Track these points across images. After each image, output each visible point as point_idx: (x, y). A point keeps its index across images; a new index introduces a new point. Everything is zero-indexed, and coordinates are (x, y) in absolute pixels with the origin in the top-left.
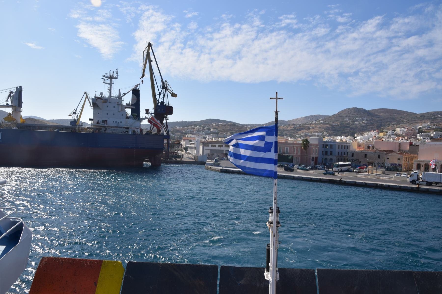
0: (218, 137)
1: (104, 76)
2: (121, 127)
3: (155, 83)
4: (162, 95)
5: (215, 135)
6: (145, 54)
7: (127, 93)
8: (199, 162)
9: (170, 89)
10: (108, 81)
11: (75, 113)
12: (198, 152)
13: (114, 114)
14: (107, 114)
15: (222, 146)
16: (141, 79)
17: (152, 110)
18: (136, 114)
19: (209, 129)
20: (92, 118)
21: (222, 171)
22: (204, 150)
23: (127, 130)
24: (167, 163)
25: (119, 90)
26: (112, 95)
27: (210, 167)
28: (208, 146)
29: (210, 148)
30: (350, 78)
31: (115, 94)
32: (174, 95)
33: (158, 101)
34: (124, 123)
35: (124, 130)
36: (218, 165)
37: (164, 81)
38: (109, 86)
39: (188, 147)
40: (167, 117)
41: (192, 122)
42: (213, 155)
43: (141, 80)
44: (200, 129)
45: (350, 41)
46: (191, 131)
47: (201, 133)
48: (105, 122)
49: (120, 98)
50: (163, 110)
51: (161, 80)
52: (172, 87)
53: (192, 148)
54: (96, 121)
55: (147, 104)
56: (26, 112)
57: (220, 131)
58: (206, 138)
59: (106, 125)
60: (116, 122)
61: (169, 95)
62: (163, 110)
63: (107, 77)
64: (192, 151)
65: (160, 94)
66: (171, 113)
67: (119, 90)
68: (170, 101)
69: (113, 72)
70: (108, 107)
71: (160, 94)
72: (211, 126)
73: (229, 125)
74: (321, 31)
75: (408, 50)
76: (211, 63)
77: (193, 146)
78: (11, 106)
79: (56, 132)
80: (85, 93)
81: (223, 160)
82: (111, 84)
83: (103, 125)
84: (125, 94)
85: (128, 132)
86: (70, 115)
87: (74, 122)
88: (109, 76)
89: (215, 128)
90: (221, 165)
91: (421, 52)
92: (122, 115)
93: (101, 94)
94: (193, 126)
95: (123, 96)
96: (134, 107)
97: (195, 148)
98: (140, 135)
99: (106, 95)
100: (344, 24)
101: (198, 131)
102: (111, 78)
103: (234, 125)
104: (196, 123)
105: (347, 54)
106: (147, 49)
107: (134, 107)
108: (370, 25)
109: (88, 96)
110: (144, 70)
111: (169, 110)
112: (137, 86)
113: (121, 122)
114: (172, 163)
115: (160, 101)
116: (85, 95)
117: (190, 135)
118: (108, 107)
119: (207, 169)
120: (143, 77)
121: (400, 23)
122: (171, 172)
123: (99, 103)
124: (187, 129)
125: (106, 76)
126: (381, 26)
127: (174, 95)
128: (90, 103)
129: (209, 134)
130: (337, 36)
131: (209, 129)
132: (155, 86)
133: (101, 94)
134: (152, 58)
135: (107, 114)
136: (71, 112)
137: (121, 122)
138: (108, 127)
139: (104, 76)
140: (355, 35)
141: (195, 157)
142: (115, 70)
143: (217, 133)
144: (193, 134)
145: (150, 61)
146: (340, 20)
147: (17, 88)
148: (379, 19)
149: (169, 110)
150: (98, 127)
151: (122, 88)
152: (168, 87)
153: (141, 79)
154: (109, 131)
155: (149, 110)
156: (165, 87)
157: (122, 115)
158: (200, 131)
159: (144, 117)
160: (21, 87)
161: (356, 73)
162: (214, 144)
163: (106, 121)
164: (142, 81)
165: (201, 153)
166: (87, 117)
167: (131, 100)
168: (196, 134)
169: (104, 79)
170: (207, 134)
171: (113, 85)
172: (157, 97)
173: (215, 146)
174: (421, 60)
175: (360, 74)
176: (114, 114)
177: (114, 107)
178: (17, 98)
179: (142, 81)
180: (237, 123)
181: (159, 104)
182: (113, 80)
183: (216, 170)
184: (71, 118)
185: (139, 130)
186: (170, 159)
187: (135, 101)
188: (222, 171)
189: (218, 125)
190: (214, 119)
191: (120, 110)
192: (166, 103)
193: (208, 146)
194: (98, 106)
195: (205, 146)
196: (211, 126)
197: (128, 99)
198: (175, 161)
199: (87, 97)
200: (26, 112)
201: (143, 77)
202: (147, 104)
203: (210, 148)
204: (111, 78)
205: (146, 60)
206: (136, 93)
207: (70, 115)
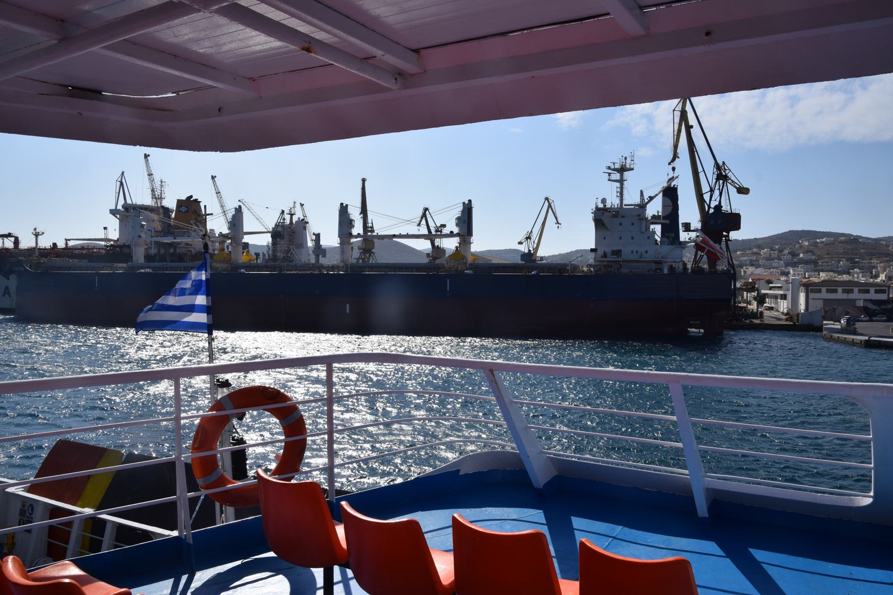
0: (819, 271)
1: (609, 168)
2: (648, 262)
3: (700, 169)
4: (717, 193)
5: (809, 266)
6: (678, 114)
7: (656, 195)
8: (796, 326)
9: (733, 178)
10: (617, 176)
11: (528, 238)
12: (795, 302)
14: (621, 238)
15: (852, 291)
16: (669, 164)
18: (673, 235)
19: (794, 254)
20: (594, 247)
21: (869, 345)
22: (810, 301)
25: (642, 192)
27: (836, 335)
28: (820, 291)
29: (824, 294)
31: (632, 198)
32: (743, 191)
33: (709, 207)
34: (651, 254)
35: (654, 266)
36: (855, 333)
37: (721, 163)
38: (618, 185)
39: (765, 294)
42: (834, 310)
43: (671, 166)
44: (773, 256)
46: (751, 261)
47: (774, 265)
48: (617, 253)
49: (643, 206)
52: (738, 173)
53: (775, 297)
54: (600, 252)
55: (689, 213)
56: (479, 244)
58: (789, 273)
60: (637, 252)
61: (733, 191)
62: (720, 222)
63: (614, 170)
64: (777, 303)
65: (712, 191)
66: (737, 227)
67: (642, 192)
68: (734, 203)
69: (626, 158)
70: (621, 224)
71: (712, 191)
72: (797, 246)
73: (841, 242)
76: (792, 106)
78: (458, 235)
79: (467, 274)
80: (547, 199)
81: (858, 321)
82: (621, 181)
84: (651, 198)
85: (661, 270)
86: (520, 243)
87: (529, 257)
89: (807, 252)
90: (860, 331)
94: (755, 250)
95: (649, 201)
96: (668, 222)
97: (784, 297)
98: (678, 275)
99: (613, 201)
101: (769, 259)
102: (622, 170)
103: (853, 241)
106: (681, 104)
107: (668, 222)
110: (676, 147)
111: (734, 221)
115: (713, 205)
116: (547, 204)
118: (621, 224)
119: (830, 339)
120: (673, 160)
123: (606, 219)
124: (743, 255)
125: (613, 167)
127: (743, 191)
129: (794, 265)
131: (794, 254)
132: (702, 175)
134: (692, 120)
136: (522, 236)
137: (646, 252)
138: (623, 261)
139: (609, 168)
142: (627, 155)
143: (815, 263)
144: (758, 266)
145: (689, 128)
147: (464, 203)
149: (734, 221)
151: (644, 187)
152: (730, 175)
153: (669, 164)
154: (624, 270)
156: (722, 176)
158: (773, 259)
160: (470, 201)
162: (831, 285)
164: (674, 169)
165: (802, 307)
166: (112, 230)
167: (660, 209)
168: (764, 266)
169: (610, 174)
170: (787, 265)
171: (625, 183)
172: (707, 197)
173: (836, 291)
177: (633, 224)
179: (674, 169)
180: (861, 237)
181: (711, 211)
182: (626, 173)
183: (853, 343)
184: (524, 248)
185: (681, 266)
187: (670, 209)
188: (869, 345)
192: (725, 208)
193: (820, 291)
195: (813, 291)
196: (797, 246)
197: (655, 208)
199: (550, 206)
200: (479, 244)
201: (673, 160)
202: (689, 213)
203: (824, 294)
204: (622, 170)
205: (680, 125)
206: (670, 193)
207: (520, 243)
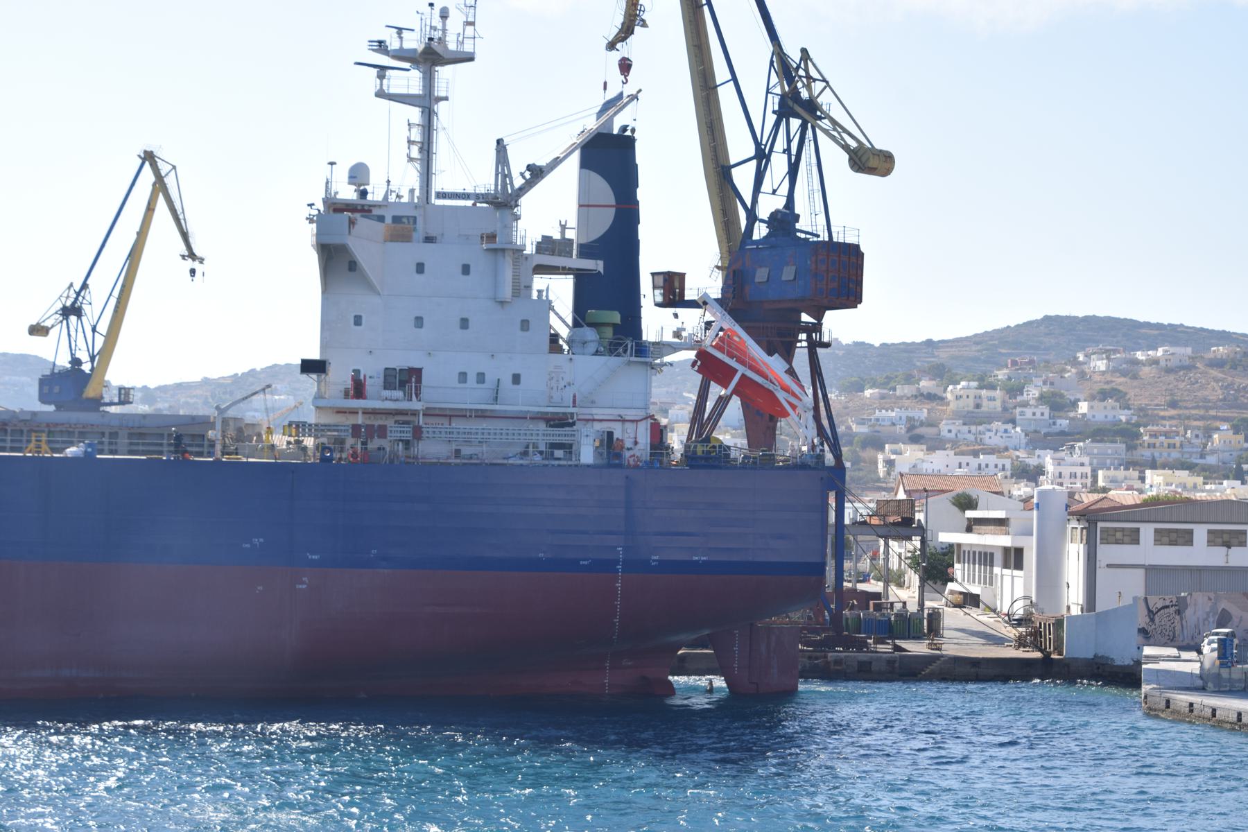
0: (1141, 466)
1: (381, 47)
3: (721, 72)
4: (779, 164)
8: (1049, 663)
10: (409, 80)
11: (72, 311)
12: (1049, 577)
13: (464, 323)
16: (611, 46)
17: (705, 280)
19: (1057, 403)
20: (315, 355)
22: (1100, 573)
23: (560, 435)
24: (830, 674)
25: (501, 145)
26: (440, 183)
31: (464, 170)
32: (869, 161)
33: (752, 217)
34: (539, 384)
35: (542, 435)
40: (817, 328)
41: (908, 349)
42: (1180, 607)
43: (615, 56)
44: (987, 406)
46: (912, 424)
47: (992, 439)
48: (406, 379)
50: (788, 273)
51: (768, 48)
52: (856, 97)
53: (985, 558)
54: (339, 376)
57: (1146, 416)
58: (1040, 470)
59: (415, 405)
60: (481, 378)
61: (835, 158)
63: (401, 55)
65: (762, 156)
67: (501, 145)
68: (842, 206)
69: (444, 15)
71: (762, 156)
72: (1071, 373)
73: (1218, 364)
77: (1005, 541)
79: (74, 459)
80: (149, 157)
82: (427, 102)
83: (394, 400)
84: (537, 173)
86: (38, 330)
88: (413, 42)
89: (1104, 395)
92: (525, 325)
93: (358, 174)
94: (926, 384)
95: (529, 185)
96: (598, 265)
97: (1014, 558)
99: (394, 179)
101: (974, 417)
102: (431, 57)
104: (943, 355)
107: (598, 265)
109: (170, 181)
112: (613, 105)
113: (516, 379)
114: (867, 672)
115: (764, 212)
116: (148, 176)
117: (910, 456)
119: (1160, 711)
120: (626, 31)
122: (862, 738)
123: (365, 243)
124: (885, 402)
127: (869, 161)
129: (1056, 440)
131: (1057, 403)
132: (726, 96)
133: (358, 174)
135: (419, 322)
136: (45, 307)
137: (516, 379)
138: (428, 413)
139: (381, 47)
141: (1031, 628)
143: (1128, 434)
144: (935, 444)
150: (360, 419)
151: (515, 118)
152: (825, 100)
153: (611, 46)
154: (432, 449)
155: (682, 277)
156: (798, 105)
157: (525, 325)
159: (668, 337)
162: (1173, 518)
163: (417, 372)
165: (1073, 598)
169: (382, 70)
171: (441, 108)
172: (743, 178)
173: (1186, 539)
176: (464, 323)
177: (466, 270)
181: (760, 231)
182: (444, 73)
184: (54, 351)
185: (644, 438)
186: (850, 643)
187: (605, 220)
189: (1131, 369)
190: (1090, 321)
191: (507, 292)
194: (353, 266)
195: (1112, 538)
196: (1071, 373)
197: (554, 209)
198: (891, 662)
199: (160, 185)
201: (626, 31)
204: (431, 57)
206: (609, 156)
207: (38, 330)
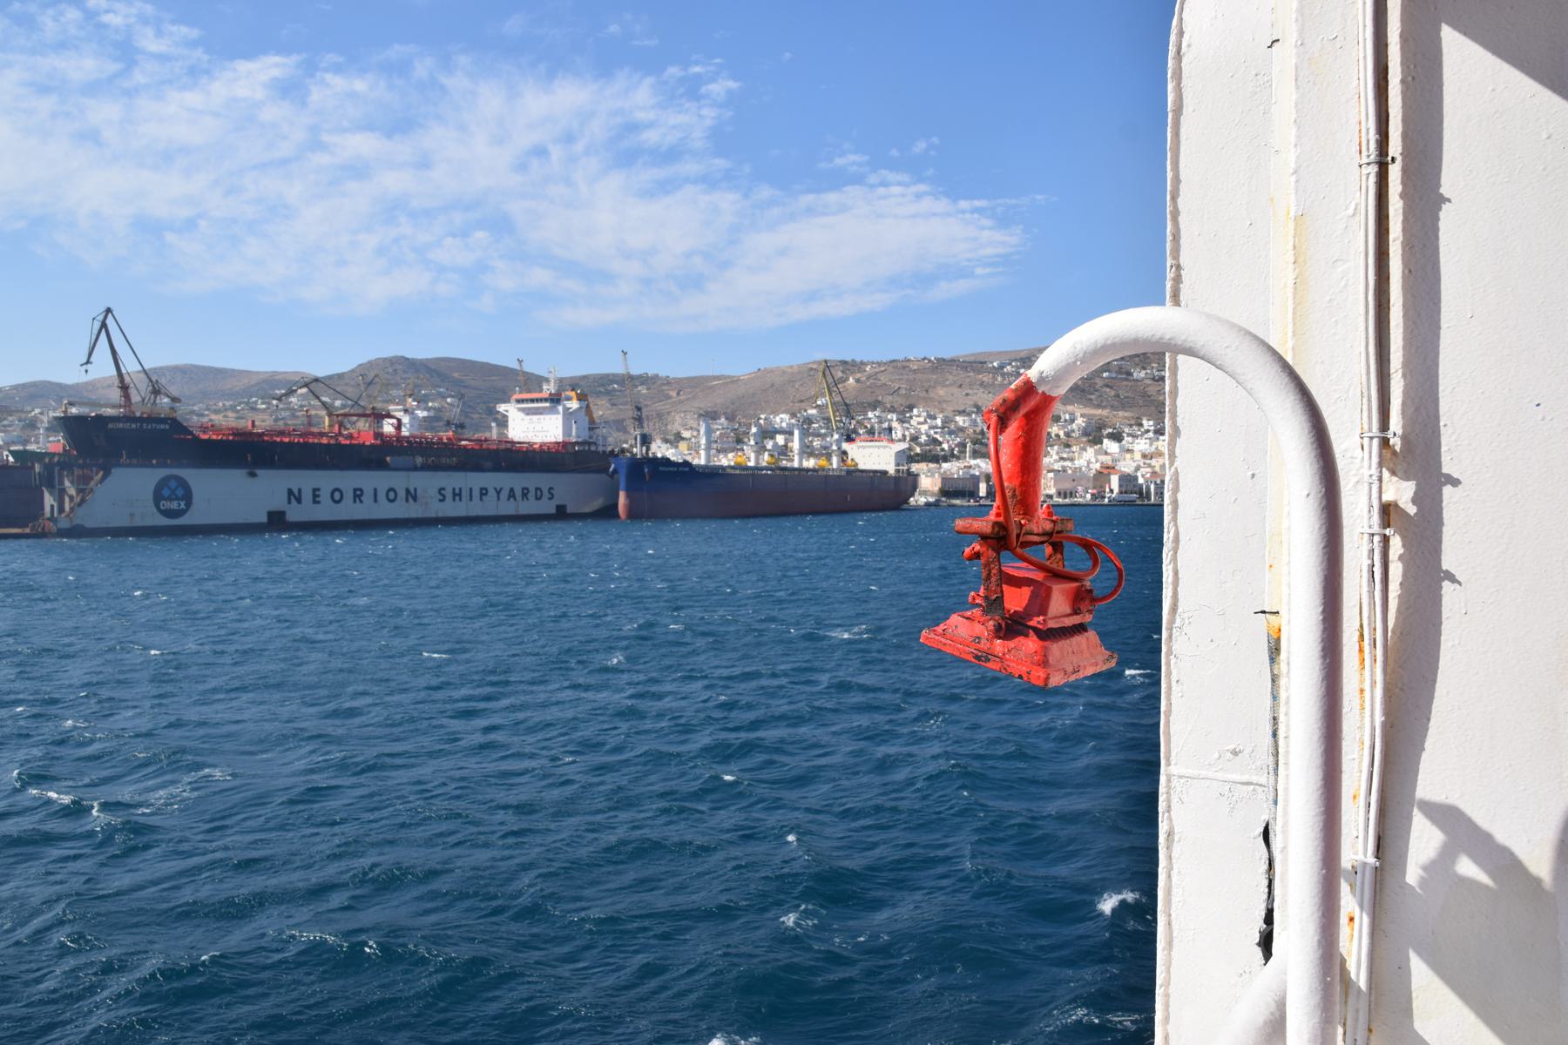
30: (170, 237)
45: (184, 113)
74: (85, 66)
75: (358, 170)
91: (394, 182)
100: (162, 58)
105: (167, 156)
108: (253, 77)
121: (338, 89)
126: (289, 90)
128: (1181, 20)
130: (131, 93)
140: (193, 98)
146: (150, 42)
148: (276, 65)
161: (191, 224)
174: (392, 210)
175: (203, 223)
178: (1455, 482)
